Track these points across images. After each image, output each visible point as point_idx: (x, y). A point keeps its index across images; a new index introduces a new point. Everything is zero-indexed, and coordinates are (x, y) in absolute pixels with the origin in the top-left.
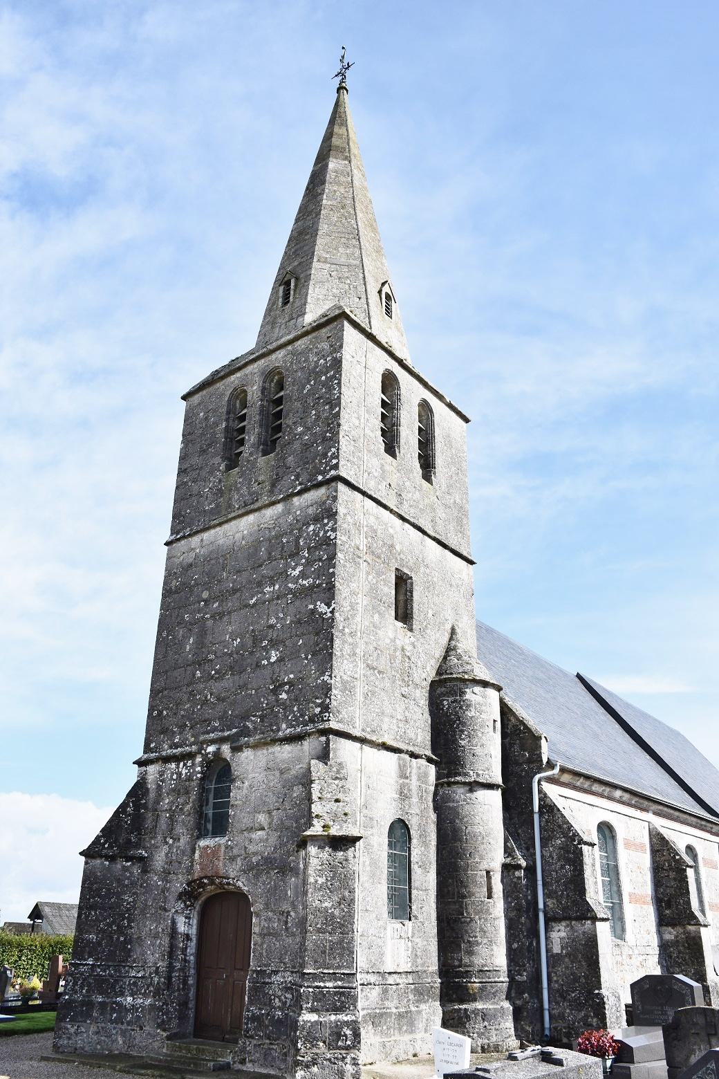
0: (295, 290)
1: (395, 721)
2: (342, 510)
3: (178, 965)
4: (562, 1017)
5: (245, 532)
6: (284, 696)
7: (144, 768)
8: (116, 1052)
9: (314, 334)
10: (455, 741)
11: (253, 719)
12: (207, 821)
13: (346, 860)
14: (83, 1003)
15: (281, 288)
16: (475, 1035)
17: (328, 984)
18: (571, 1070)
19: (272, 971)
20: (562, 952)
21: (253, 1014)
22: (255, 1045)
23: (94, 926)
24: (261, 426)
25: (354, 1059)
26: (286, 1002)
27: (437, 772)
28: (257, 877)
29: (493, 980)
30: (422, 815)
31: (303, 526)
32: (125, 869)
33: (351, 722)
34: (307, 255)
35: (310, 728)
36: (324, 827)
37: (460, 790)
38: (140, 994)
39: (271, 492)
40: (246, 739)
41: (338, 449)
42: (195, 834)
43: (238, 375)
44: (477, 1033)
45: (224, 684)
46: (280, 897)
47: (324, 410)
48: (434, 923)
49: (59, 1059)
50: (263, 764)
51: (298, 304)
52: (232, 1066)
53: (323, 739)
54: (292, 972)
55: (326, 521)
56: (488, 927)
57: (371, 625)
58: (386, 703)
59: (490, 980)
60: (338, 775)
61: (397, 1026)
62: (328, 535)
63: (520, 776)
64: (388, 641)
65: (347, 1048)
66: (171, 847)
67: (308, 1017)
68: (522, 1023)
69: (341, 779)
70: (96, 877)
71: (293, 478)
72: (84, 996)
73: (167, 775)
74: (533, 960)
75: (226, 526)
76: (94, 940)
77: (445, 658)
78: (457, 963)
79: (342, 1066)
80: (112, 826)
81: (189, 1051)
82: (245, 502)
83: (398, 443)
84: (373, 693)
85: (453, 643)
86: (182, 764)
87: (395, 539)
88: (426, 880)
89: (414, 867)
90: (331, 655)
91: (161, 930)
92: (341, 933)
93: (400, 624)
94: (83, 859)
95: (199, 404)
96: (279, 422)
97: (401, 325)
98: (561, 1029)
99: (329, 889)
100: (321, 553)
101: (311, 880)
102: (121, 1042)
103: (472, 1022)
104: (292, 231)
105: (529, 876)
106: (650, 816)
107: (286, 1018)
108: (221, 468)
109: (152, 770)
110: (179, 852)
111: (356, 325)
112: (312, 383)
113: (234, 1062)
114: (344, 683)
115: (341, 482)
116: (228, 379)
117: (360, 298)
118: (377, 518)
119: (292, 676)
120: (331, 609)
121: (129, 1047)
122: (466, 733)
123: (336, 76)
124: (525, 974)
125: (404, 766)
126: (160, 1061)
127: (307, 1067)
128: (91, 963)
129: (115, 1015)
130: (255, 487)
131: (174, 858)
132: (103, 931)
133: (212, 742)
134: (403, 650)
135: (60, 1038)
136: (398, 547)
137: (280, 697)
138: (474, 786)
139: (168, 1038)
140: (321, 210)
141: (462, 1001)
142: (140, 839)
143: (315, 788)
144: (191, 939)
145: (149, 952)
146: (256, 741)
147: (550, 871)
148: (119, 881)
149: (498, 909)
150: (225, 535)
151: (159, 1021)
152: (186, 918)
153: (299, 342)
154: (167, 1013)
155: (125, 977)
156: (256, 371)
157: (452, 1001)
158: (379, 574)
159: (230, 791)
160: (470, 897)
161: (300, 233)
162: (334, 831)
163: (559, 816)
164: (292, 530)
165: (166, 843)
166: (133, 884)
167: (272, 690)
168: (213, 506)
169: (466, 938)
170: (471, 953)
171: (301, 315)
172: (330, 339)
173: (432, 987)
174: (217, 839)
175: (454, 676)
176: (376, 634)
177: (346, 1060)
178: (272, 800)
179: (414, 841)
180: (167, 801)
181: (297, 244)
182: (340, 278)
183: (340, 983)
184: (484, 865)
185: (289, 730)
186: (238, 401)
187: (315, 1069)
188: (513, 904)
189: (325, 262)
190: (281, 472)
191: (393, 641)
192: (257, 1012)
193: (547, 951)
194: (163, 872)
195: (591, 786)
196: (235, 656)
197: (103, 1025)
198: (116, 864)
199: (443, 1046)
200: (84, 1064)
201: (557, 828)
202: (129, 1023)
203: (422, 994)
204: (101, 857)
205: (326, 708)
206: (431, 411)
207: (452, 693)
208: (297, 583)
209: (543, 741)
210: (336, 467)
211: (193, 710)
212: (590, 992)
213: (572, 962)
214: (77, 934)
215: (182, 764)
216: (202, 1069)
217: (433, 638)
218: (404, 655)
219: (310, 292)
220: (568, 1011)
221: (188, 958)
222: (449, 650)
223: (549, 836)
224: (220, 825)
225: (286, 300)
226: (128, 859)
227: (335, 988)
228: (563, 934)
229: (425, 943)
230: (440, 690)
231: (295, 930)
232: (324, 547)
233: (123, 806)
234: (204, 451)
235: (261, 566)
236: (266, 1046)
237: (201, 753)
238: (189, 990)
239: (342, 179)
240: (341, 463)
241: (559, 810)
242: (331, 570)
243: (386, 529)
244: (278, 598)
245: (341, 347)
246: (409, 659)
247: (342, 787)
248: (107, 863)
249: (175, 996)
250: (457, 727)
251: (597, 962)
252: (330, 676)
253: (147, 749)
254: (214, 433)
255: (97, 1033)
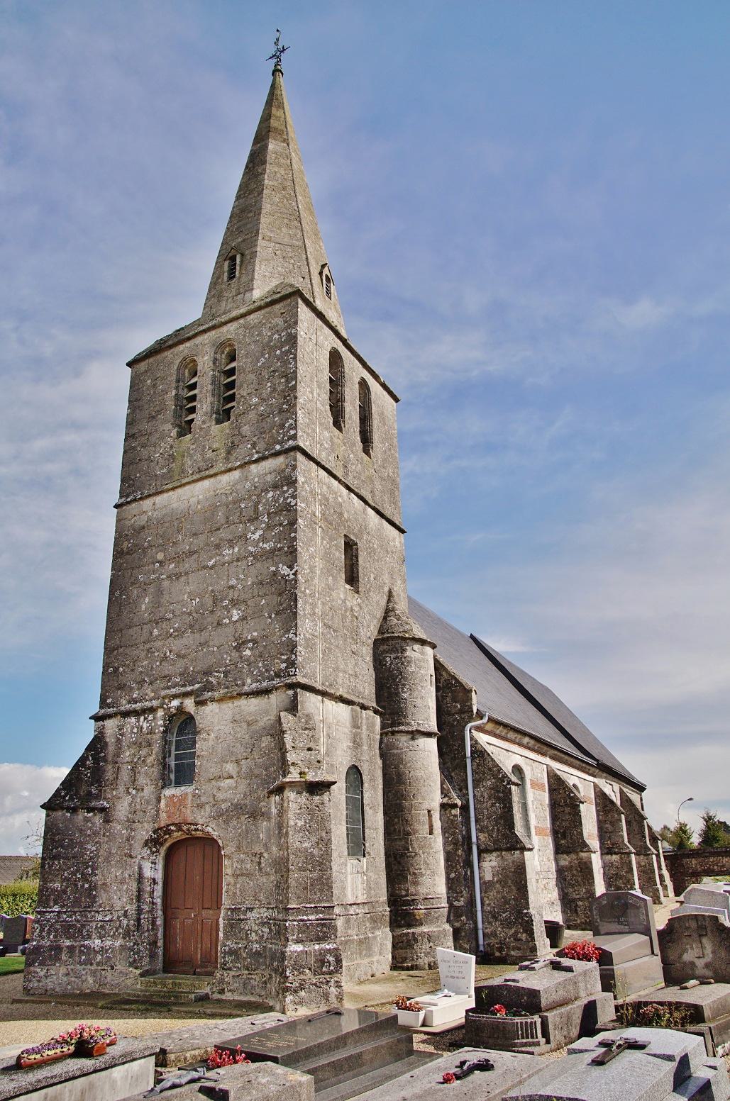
0: (241, 266)
1: (347, 676)
2: (301, 479)
3: (146, 908)
4: (494, 934)
5: (201, 497)
6: (248, 652)
7: (101, 723)
8: (87, 991)
9: (267, 310)
10: (397, 694)
11: (216, 674)
12: (170, 771)
13: (323, 804)
14: (51, 948)
15: (227, 263)
16: (423, 955)
17: (310, 918)
18: (580, 975)
19: (247, 908)
20: (493, 879)
21: (230, 949)
22: (233, 976)
23: (58, 875)
24: (213, 395)
25: (337, 982)
26: (263, 935)
27: (381, 722)
28: (227, 822)
29: (436, 906)
30: (371, 761)
31: (262, 492)
32: (87, 820)
33: (313, 676)
34: (251, 233)
35: (276, 682)
36: (300, 774)
37: (403, 739)
38: (109, 936)
39: (227, 459)
40: (210, 693)
41: (296, 421)
42: (160, 784)
43: (188, 344)
44: (424, 953)
45: (185, 641)
46: (252, 840)
47: (280, 383)
48: (383, 858)
49: (33, 1000)
50: (229, 716)
51: (244, 279)
52: (210, 997)
53: (291, 692)
54: (268, 908)
55: (285, 488)
56: (431, 860)
57: (327, 587)
58: (340, 659)
59: (433, 906)
60: (307, 726)
61: (358, 951)
62: (288, 501)
63: (453, 726)
64: (340, 602)
65: (331, 973)
66: (134, 797)
67: (294, 948)
68: (461, 942)
69: (310, 729)
70: (58, 829)
71: (249, 446)
72: (51, 941)
73: (127, 729)
74: (468, 887)
75: (179, 491)
76: (59, 889)
77: (385, 618)
78: (404, 893)
79: (326, 989)
80: (72, 779)
81: (165, 985)
82: (199, 468)
83: (343, 417)
84: (330, 650)
85: (391, 604)
86: (142, 718)
87: (343, 508)
88: (375, 819)
89: (366, 808)
90: (295, 614)
91: (127, 876)
92: (320, 870)
93: (348, 587)
94: (44, 811)
95: (146, 371)
96: (231, 392)
97: (338, 307)
98: (494, 945)
99: (308, 831)
100: (282, 518)
101: (292, 823)
102: (91, 982)
103: (419, 944)
104: (233, 208)
105: (464, 814)
106: (547, 761)
107: (265, 950)
108: (172, 434)
109: (111, 725)
110: (143, 801)
111: (309, 304)
112: (267, 356)
113: (213, 993)
114: (306, 639)
115: (301, 453)
116: (177, 348)
117: (304, 278)
118: (329, 487)
119: (255, 634)
120: (293, 571)
121: (100, 985)
122: (407, 686)
123: (271, 58)
124: (462, 899)
125: (357, 716)
126: (139, 996)
127: (296, 992)
128: (57, 910)
129: (83, 957)
130: (210, 454)
131: (138, 807)
132: (68, 880)
133: (175, 697)
134: (352, 610)
135: (30, 981)
136: (346, 515)
137: (244, 653)
138: (415, 734)
139: (142, 975)
140: (263, 190)
141: (409, 926)
142: (100, 791)
143: (288, 738)
144: (157, 883)
145: (115, 897)
146: (222, 695)
147: (482, 809)
148: (81, 831)
149: (438, 844)
150: (179, 499)
151: (131, 960)
152: (152, 863)
153: (252, 316)
154: (138, 953)
155: (91, 921)
156: (207, 341)
157: (400, 926)
158: (331, 539)
159: (195, 742)
160: (414, 833)
161: (243, 211)
162: (311, 777)
163: (490, 760)
164: (250, 496)
165: (129, 793)
166: (95, 834)
167: (235, 648)
168: (165, 471)
169: (412, 870)
170: (416, 883)
171: (248, 290)
172: (284, 315)
173: (383, 915)
174: (183, 788)
175: (396, 635)
176: (331, 595)
177: (330, 984)
178: (240, 750)
179: (366, 785)
180: (128, 754)
181: (240, 221)
182: (284, 257)
183: (321, 916)
184: (426, 806)
185: (254, 685)
186: (187, 371)
187: (303, 993)
188: (450, 839)
189: (270, 240)
190: (236, 440)
191: (344, 601)
192: (234, 946)
193: (480, 878)
194: (128, 821)
195: (507, 733)
196: (194, 615)
197: (72, 967)
198: (78, 815)
199: (449, 964)
200: (61, 1004)
201: (486, 771)
202: (98, 964)
203: (376, 922)
204: (62, 808)
205: (292, 664)
206: (368, 389)
207: (394, 650)
208: (257, 546)
209: (473, 693)
210: (294, 437)
211: (152, 667)
212: (520, 912)
213: (503, 887)
214: (41, 883)
215: (142, 718)
216: (183, 1001)
217: (375, 600)
218: (353, 616)
219: (257, 268)
220: (500, 929)
221: (155, 901)
222: (388, 612)
223: (480, 778)
224: (184, 774)
225: (232, 275)
226: (90, 810)
227: (317, 920)
228: (494, 864)
229: (376, 876)
230: (382, 648)
231: (268, 869)
232: (284, 513)
233: (83, 760)
234: (153, 417)
235: (219, 529)
236: (245, 977)
237: (163, 707)
238: (157, 929)
239: (282, 161)
240: (300, 434)
241: (489, 755)
242: (293, 535)
243: (336, 498)
244: (238, 560)
245: (296, 323)
246: (357, 619)
247: (312, 737)
248: (69, 815)
249: (145, 936)
250: (400, 682)
251: (525, 887)
252: (295, 634)
253: (103, 703)
254: (163, 402)
255: (67, 974)
